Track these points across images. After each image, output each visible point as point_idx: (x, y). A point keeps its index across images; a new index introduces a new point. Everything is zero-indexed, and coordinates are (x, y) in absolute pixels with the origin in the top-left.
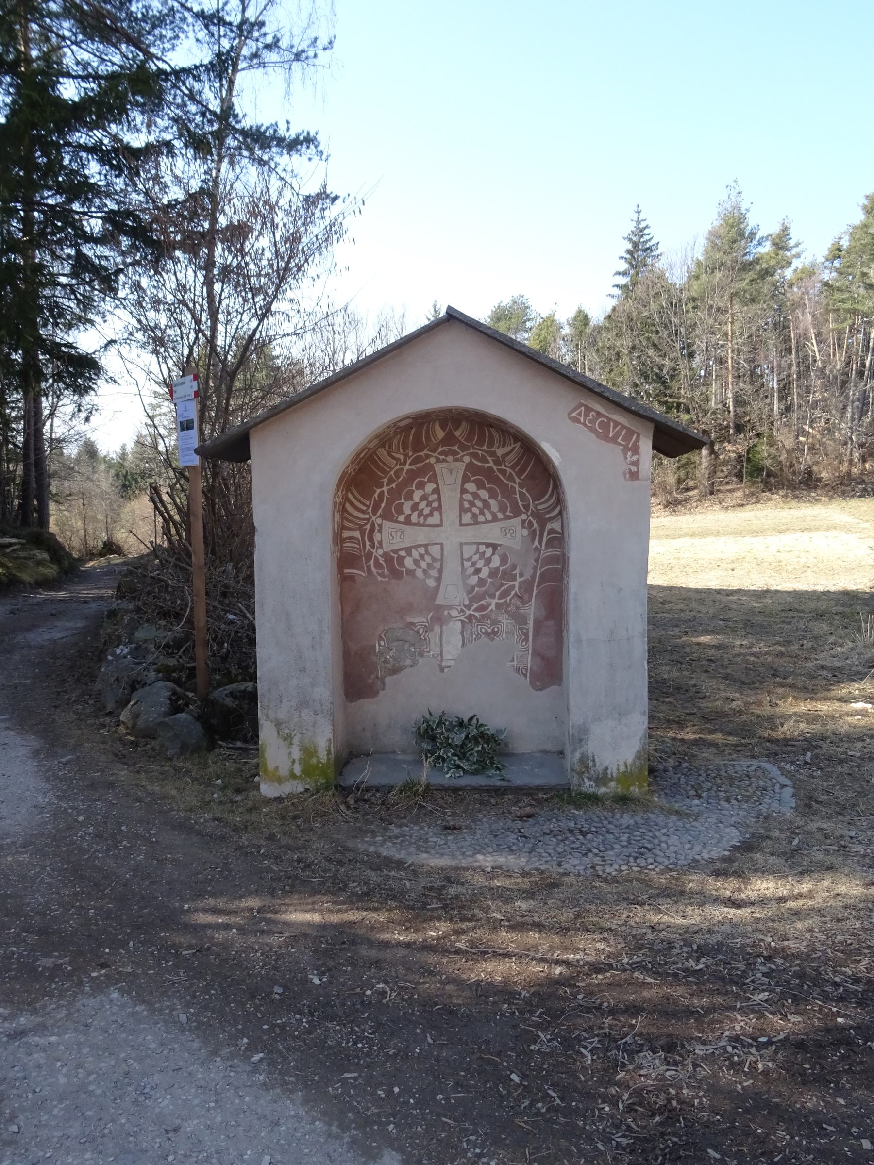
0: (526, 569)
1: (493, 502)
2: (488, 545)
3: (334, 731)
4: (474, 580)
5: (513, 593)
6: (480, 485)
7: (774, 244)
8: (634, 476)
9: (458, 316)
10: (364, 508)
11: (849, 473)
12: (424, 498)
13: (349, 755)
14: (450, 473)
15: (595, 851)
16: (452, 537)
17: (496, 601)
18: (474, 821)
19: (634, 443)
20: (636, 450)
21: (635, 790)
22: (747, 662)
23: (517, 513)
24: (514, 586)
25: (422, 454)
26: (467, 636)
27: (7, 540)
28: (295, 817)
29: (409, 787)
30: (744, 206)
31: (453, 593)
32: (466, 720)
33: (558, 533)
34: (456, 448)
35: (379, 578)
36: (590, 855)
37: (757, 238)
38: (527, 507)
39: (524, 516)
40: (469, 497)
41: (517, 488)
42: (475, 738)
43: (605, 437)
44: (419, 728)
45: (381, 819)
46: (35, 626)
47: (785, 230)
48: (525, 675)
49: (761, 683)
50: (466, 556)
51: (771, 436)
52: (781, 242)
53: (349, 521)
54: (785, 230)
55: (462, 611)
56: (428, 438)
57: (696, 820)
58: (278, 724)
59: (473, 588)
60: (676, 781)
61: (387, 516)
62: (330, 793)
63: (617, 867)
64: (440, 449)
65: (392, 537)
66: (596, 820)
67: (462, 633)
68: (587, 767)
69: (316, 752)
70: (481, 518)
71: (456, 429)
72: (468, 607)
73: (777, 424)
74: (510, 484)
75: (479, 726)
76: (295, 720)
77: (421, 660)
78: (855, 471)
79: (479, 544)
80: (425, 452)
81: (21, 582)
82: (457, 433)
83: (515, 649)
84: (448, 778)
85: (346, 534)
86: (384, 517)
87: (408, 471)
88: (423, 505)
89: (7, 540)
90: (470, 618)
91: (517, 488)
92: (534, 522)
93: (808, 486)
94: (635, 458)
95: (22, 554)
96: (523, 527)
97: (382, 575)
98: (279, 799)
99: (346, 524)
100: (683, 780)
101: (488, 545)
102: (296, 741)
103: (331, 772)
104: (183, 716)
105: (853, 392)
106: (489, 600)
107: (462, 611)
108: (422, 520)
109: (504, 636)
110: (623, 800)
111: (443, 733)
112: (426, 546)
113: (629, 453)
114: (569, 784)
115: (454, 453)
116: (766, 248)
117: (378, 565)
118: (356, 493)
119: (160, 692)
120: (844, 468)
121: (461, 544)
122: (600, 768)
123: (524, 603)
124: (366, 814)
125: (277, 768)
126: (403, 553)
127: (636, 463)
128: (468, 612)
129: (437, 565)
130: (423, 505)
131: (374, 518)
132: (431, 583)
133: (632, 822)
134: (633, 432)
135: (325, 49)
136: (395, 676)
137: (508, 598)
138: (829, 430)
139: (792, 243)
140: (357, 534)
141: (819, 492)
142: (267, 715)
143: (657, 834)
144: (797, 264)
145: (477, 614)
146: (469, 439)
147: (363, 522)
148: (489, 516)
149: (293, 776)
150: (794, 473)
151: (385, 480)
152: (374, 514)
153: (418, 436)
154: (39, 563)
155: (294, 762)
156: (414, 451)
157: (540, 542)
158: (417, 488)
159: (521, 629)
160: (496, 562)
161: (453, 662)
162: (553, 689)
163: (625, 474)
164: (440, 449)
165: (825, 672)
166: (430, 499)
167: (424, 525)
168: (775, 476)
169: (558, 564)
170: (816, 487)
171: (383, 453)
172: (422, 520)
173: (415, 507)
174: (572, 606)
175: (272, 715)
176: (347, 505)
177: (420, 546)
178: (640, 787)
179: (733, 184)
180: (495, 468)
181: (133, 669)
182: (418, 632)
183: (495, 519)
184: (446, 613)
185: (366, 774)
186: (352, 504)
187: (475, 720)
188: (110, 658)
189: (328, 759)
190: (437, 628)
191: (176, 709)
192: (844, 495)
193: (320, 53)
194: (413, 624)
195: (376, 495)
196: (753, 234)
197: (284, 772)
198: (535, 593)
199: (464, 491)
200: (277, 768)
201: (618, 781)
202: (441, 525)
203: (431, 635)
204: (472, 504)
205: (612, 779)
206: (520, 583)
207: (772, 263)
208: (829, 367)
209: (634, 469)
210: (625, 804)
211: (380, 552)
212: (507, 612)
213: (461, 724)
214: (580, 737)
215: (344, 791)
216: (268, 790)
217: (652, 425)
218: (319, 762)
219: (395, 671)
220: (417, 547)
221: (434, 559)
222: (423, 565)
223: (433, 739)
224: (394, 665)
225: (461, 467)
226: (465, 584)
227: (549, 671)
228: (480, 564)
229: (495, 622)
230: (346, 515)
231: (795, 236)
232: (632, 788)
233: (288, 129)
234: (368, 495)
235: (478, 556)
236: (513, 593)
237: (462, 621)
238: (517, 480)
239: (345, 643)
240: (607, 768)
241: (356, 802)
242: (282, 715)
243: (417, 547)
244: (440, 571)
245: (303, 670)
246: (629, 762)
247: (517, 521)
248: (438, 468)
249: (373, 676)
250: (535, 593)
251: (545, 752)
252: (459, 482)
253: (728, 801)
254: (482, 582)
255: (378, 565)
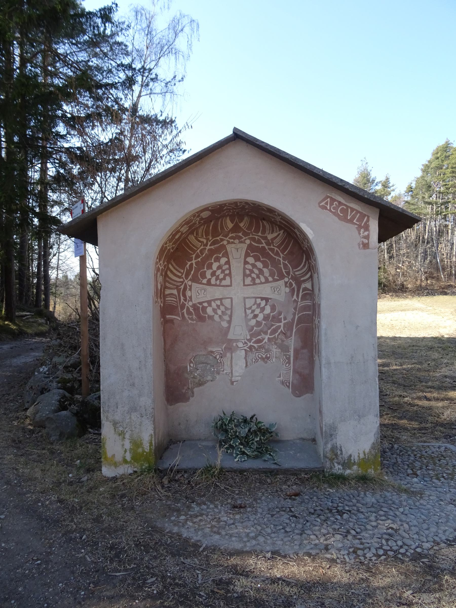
0: (289, 315)
1: (265, 270)
2: (262, 299)
3: (155, 429)
4: (253, 322)
5: (279, 331)
6: (257, 259)
7: (383, 185)
8: (366, 246)
9: (241, 134)
10: (180, 275)
11: (421, 285)
12: (219, 267)
13: (167, 444)
14: (237, 251)
15: (353, 532)
16: (238, 293)
17: (268, 336)
18: (255, 500)
19: (366, 223)
20: (367, 228)
21: (371, 472)
22: (402, 373)
23: (281, 277)
24: (280, 326)
25: (218, 238)
26: (249, 360)
27: (24, 313)
28: (123, 496)
29: (208, 469)
30: (369, 169)
31: (239, 331)
32: (248, 418)
33: (309, 290)
34: (240, 234)
35: (190, 321)
36: (350, 537)
37: (375, 182)
38: (288, 273)
39: (286, 279)
40: (249, 267)
41: (282, 261)
42: (255, 432)
43: (344, 219)
44: (217, 423)
45: (186, 498)
46: (19, 355)
47: (387, 179)
48: (289, 387)
49: (415, 386)
50: (248, 306)
51: (384, 269)
52: (386, 185)
53: (170, 283)
54: (387, 179)
55: (246, 343)
56: (222, 228)
57: (421, 498)
58: (115, 424)
59: (252, 328)
60: (394, 461)
61: (195, 280)
62: (151, 475)
63: (374, 551)
64: (230, 235)
65: (198, 294)
66: (347, 498)
67: (245, 358)
68: (336, 455)
69: (142, 444)
70: (257, 281)
71: (241, 222)
72: (250, 340)
73: (387, 263)
74: (277, 258)
75: (258, 423)
76: (127, 421)
77: (218, 377)
78: (423, 284)
79: (256, 298)
80: (220, 237)
81: (26, 333)
82: (242, 225)
83: (281, 367)
84: (236, 462)
85: (168, 292)
86: (193, 280)
87: (209, 250)
88: (219, 272)
89: (24, 313)
90: (251, 347)
91: (282, 261)
92: (293, 283)
93: (402, 291)
94: (366, 233)
95: (31, 320)
96: (286, 286)
97: (192, 319)
98: (114, 479)
99: (167, 285)
100: (399, 460)
101: (262, 299)
102: (127, 436)
103: (152, 459)
104: (64, 413)
105: (421, 250)
106: (263, 335)
107: (246, 343)
108: (218, 282)
109: (274, 360)
110: (363, 479)
111: (232, 429)
112: (221, 299)
113: (362, 230)
114: (324, 467)
115: (240, 238)
116: (379, 187)
117: (189, 313)
118: (174, 265)
119: (54, 397)
120: (418, 283)
121: (245, 298)
122: (346, 456)
123: (287, 337)
124: (176, 492)
125: (114, 456)
126: (205, 304)
127: (367, 237)
128: (249, 344)
129: (229, 312)
130: (219, 272)
131: (186, 281)
132: (225, 324)
133: (373, 500)
134: (365, 215)
135: (179, 81)
136: (201, 388)
137: (277, 334)
138: (410, 267)
139: (391, 185)
140: (175, 292)
141: (407, 294)
142: (107, 418)
143: (398, 513)
144: (393, 194)
145: (255, 345)
146: (249, 228)
147: (179, 284)
148: (263, 280)
149: (125, 461)
150: (396, 285)
151: (194, 256)
152: (187, 279)
153: (215, 227)
154: (40, 324)
155: (126, 451)
156: (213, 237)
157: (298, 296)
158: (215, 261)
159: (285, 355)
160: (268, 310)
161: (239, 378)
162: (307, 396)
163: (359, 245)
164: (230, 235)
165: (447, 379)
166: (223, 268)
167: (219, 286)
168: (387, 287)
169: (310, 311)
170: (406, 292)
171: (192, 238)
172: (218, 282)
173: (213, 274)
174: (323, 338)
175: (111, 418)
176: (169, 273)
177: (217, 299)
178: (375, 470)
179: (364, 160)
180: (267, 247)
181: (43, 381)
182: (215, 358)
183: (267, 281)
184: (234, 344)
185: (176, 460)
186: (171, 272)
187: (254, 418)
188: (36, 373)
189: (150, 449)
190: (228, 355)
191: (62, 407)
192: (419, 295)
193: (177, 84)
194: (212, 352)
195: (188, 266)
196: (373, 181)
197: (119, 458)
198: (294, 330)
199: (246, 263)
200: (114, 456)
201: (359, 465)
202: (231, 286)
203: (225, 359)
204: (251, 271)
205: (354, 464)
206: (284, 324)
207: (382, 193)
208: (409, 238)
209: (366, 241)
210: (365, 483)
211: (190, 303)
212: (276, 344)
213: (245, 421)
214: (331, 434)
215: (160, 473)
216: (107, 471)
217: (378, 210)
218: (144, 451)
219: (200, 384)
220: (215, 300)
221: (226, 308)
222: (219, 312)
223: (226, 431)
224: (200, 380)
225: (244, 247)
226: (247, 325)
227: (305, 383)
228: (257, 311)
229: (268, 351)
230: (167, 279)
231: (392, 182)
232: (369, 470)
233: (161, 115)
234: (182, 266)
235: (256, 306)
236: (279, 331)
237: (245, 350)
238: (282, 255)
239: (166, 365)
240: (350, 456)
241: (169, 482)
242: (117, 417)
243: (215, 300)
244: (231, 316)
245: (133, 385)
246: (367, 451)
247: (282, 283)
248: (229, 247)
249: (186, 388)
250: (294, 330)
251: (303, 439)
252: (243, 257)
253: (438, 479)
254: (258, 324)
255: (189, 313)
